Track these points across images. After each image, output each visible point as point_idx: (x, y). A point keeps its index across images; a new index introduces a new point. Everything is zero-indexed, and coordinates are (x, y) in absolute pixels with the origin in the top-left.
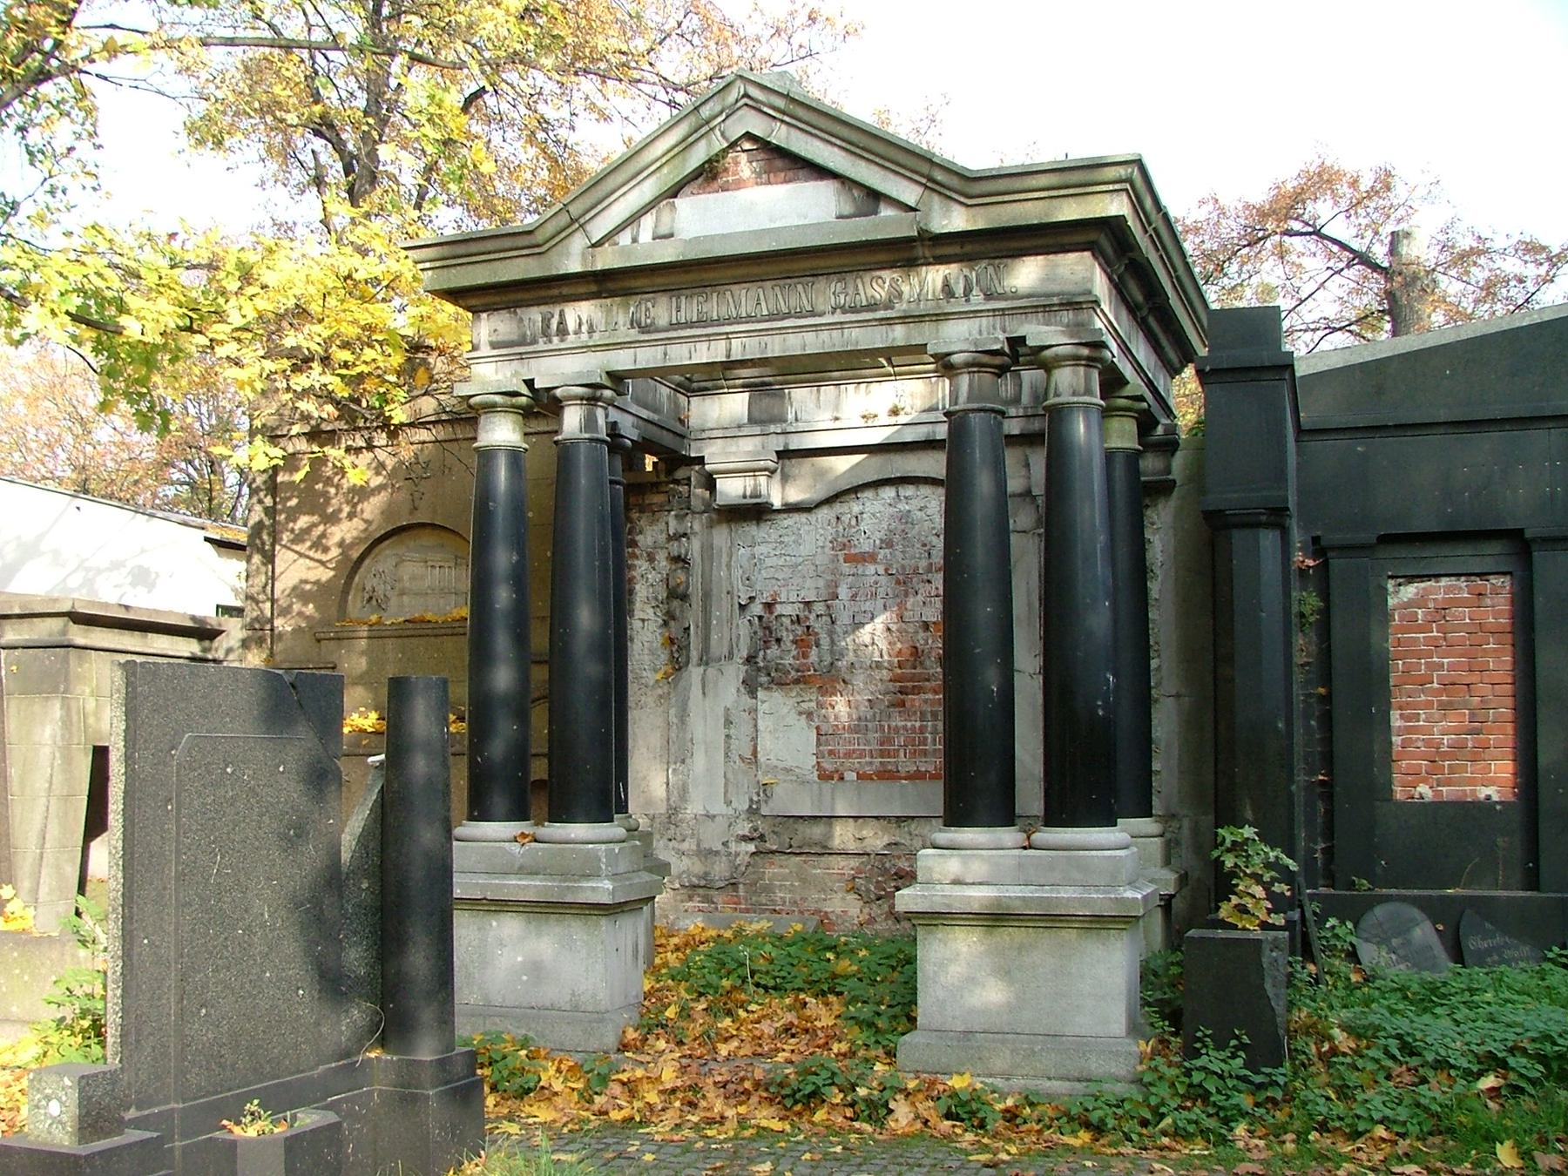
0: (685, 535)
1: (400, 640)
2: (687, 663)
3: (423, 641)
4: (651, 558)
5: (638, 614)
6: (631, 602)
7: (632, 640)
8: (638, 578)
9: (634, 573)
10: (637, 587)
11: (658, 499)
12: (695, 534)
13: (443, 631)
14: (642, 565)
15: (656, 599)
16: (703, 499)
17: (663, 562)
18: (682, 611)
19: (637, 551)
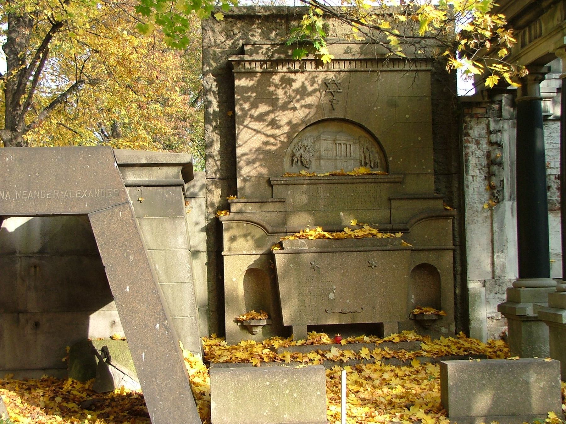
0: (499, 131)
1: (328, 186)
2: (503, 199)
3: (344, 186)
4: (478, 143)
5: (471, 173)
6: (467, 166)
7: (468, 187)
8: (470, 153)
9: (468, 151)
10: (470, 158)
11: (480, 111)
12: (505, 130)
13: (358, 181)
14: (472, 147)
15: (481, 165)
16: (509, 111)
17: (484, 145)
18: (499, 172)
19: (470, 139)
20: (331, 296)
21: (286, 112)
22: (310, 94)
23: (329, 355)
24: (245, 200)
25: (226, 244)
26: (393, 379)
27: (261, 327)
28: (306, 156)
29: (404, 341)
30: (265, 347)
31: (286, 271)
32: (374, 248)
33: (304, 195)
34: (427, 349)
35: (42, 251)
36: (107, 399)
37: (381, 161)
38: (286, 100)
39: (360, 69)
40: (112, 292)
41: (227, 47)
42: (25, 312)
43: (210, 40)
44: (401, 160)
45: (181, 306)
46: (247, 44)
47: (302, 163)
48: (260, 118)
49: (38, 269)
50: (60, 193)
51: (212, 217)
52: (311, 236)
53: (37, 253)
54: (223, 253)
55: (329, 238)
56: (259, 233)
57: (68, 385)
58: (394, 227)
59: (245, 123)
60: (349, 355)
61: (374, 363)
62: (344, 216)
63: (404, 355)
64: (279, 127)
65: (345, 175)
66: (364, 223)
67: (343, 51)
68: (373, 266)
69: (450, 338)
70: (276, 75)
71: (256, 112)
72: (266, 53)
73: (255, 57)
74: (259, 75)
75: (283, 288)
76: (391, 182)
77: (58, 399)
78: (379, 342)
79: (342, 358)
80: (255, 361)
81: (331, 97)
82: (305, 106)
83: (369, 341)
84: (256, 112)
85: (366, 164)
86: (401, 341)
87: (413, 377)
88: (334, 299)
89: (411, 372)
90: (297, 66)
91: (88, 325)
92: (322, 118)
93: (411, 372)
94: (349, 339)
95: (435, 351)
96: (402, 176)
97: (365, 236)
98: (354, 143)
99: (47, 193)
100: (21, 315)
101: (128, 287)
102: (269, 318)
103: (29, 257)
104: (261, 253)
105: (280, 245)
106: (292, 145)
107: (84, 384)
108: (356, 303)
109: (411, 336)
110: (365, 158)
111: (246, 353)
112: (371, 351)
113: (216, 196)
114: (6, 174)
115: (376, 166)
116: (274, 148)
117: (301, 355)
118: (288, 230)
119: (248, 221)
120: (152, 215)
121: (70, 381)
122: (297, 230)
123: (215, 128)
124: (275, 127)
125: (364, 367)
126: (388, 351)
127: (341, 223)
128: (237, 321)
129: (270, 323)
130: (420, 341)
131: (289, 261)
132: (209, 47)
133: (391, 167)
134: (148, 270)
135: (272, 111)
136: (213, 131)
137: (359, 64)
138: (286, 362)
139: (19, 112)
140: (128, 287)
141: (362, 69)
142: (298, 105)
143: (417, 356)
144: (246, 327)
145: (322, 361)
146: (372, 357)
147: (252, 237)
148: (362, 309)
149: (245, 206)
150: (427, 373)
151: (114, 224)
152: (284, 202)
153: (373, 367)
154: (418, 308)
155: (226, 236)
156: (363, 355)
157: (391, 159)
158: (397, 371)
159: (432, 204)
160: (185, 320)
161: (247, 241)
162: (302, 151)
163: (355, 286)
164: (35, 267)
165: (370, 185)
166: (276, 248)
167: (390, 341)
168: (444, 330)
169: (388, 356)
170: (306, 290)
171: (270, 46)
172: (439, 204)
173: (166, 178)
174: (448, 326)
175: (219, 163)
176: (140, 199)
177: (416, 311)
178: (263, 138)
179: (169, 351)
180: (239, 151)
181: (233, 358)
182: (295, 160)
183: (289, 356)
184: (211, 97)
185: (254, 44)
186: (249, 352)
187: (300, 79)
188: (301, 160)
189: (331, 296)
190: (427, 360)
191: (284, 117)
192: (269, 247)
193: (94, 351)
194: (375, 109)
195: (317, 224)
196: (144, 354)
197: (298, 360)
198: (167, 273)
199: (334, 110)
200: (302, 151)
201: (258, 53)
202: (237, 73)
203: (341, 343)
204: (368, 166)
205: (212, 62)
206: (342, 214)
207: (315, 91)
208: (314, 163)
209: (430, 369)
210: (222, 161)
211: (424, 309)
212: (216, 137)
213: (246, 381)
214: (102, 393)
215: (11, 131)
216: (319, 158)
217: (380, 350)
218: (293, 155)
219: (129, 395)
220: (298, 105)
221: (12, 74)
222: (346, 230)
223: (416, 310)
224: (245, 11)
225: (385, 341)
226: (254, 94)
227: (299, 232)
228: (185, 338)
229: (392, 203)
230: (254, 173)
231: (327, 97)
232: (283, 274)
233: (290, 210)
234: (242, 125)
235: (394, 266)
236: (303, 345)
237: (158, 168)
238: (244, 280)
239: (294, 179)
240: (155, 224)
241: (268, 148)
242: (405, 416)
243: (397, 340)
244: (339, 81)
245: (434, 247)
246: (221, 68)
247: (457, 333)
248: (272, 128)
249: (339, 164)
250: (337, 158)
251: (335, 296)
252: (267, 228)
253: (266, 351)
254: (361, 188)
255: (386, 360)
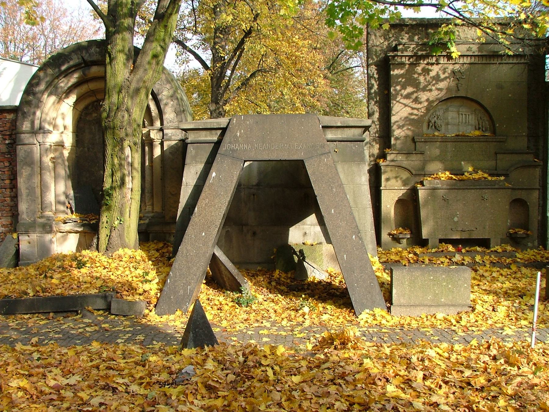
1: (454, 144)
3: (464, 144)
13: (475, 140)
20: (456, 219)
21: (425, 93)
22: (442, 80)
23: (454, 260)
24: (397, 152)
25: (383, 183)
26: (500, 277)
27: (406, 239)
28: (439, 122)
29: (505, 251)
30: (410, 253)
31: (426, 202)
32: (487, 187)
33: (437, 150)
34: (520, 257)
35: (258, 185)
36: (305, 285)
37: (490, 126)
38: (426, 84)
39: (477, 62)
40: (323, 213)
41: (385, 47)
42: (247, 225)
43: (373, 41)
45: (365, 224)
46: (400, 44)
47: (435, 127)
48: (408, 96)
49: (255, 196)
50: (284, 145)
51: (372, 163)
52: (443, 177)
53: (255, 186)
54: (381, 188)
55: (455, 179)
56: (405, 175)
57: (277, 273)
59: (398, 99)
60: (468, 259)
61: (485, 265)
62: (464, 164)
63: (505, 260)
64: (420, 103)
65: (465, 136)
66: (478, 169)
67: (465, 49)
69: (534, 250)
70: (419, 66)
71: (405, 92)
72: (413, 51)
73: (405, 54)
74: (407, 66)
75: (423, 213)
76: (498, 142)
77: (274, 283)
78: (488, 251)
79: (463, 261)
80: (404, 262)
81: (457, 82)
82: (438, 89)
83: (480, 251)
84: (405, 92)
85: (479, 129)
86: (503, 251)
87: (513, 276)
88: (457, 221)
89: (511, 272)
90: (434, 60)
91: (288, 235)
92: (450, 96)
93: (511, 272)
94: (467, 249)
95: (526, 258)
97: (479, 179)
98: (472, 114)
99: (275, 146)
100: (244, 227)
101: (333, 210)
102: (411, 233)
103: (250, 188)
104: (408, 188)
105: (422, 183)
106: (429, 114)
107: (287, 274)
109: (509, 248)
110: (479, 124)
111: (397, 256)
112: (482, 257)
113: (376, 150)
114: (248, 133)
115: (486, 130)
116: (416, 117)
117: (435, 258)
118: (427, 173)
119: (399, 167)
120: (344, 161)
121: (277, 272)
122: (433, 173)
123: (376, 102)
124: (417, 102)
125: (478, 268)
126: (494, 258)
127: (462, 169)
128: (390, 234)
129: (412, 236)
130: (515, 251)
131: (428, 195)
132: (373, 46)
134: (346, 198)
135: (416, 92)
136: (374, 105)
137: (477, 58)
138: (425, 263)
139: (220, 91)
140: (333, 210)
141: (479, 62)
142: (434, 88)
143: (515, 262)
144: (396, 239)
145: (450, 264)
146: (483, 261)
147: (401, 178)
149: (396, 156)
150: (522, 274)
151: (322, 167)
152: (423, 154)
153: (485, 269)
154: (512, 229)
155: (383, 177)
156: (477, 260)
157: (497, 125)
158: (502, 272)
159: (525, 157)
160: (368, 233)
161: (397, 181)
162: (435, 118)
164: (254, 195)
165: (483, 143)
166: (419, 185)
167: (495, 251)
168: (530, 244)
169: (494, 261)
170: (439, 215)
171: (415, 46)
172: (530, 158)
173: (353, 136)
174: (533, 242)
175: (378, 127)
176: (336, 150)
177: (511, 231)
178: (409, 110)
179: (362, 254)
180: (393, 119)
181: (389, 260)
182: (431, 125)
183: (427, 259)
184: (373, 82)
185: (404, 44)
186: (399, 256)
187: (435, 70)
188: (435, 125)
189: (456, 219)
190: (521, 264)
191: (424, 96)
192: (413, 184)
193: (295, 253)
194: (488, 90)
195: (445, 170)
196: (345, 255)
197: (433, 262)
198: (355, 201)
199: (459, 90)
200: (435, 118)
201: (407, 51)
202: (393, 64)
203: (462, 252)
204: (481, 130)
205: (374, 57)
206: (463, 163)
207: (446, 78)
208: (443, 127)
209: (524, 271)
210: (380, 125)
211: (517, 230)
212: (376, 108)
213: (417, 276)
214: (300, 281)
215: (216, 104)
216: (447, 124)
217: (488, 257)
218: (429, 122)
219: (320, 282)
220: (434, 88)
221: (217, 66)
222: (466, 174)
223: (511, 230)
224: (398, 21)
225: (492, 251)
226: (403, 80)
227: (434, 175)
228: (367, 245)
230: (403, 134)
231: (453, 82)
232: (423, 203)
234: (395, 100)
236: (436, 252)
237: (348, 129)
238: (395, 207)
239: (430, 138)
240: (346, 167)
241: (413, 117)
242: (522, 303)
243: (500, 250)
244: (463, 71)
245: (525, 187)
246: (380, 61)
247: (538, 247)
248: (416, 103)
249: (461, 128)
250: (460, 124)
252: (412, 171)
253: (411, 255)
254: (476, 145)
255: (493, 264)
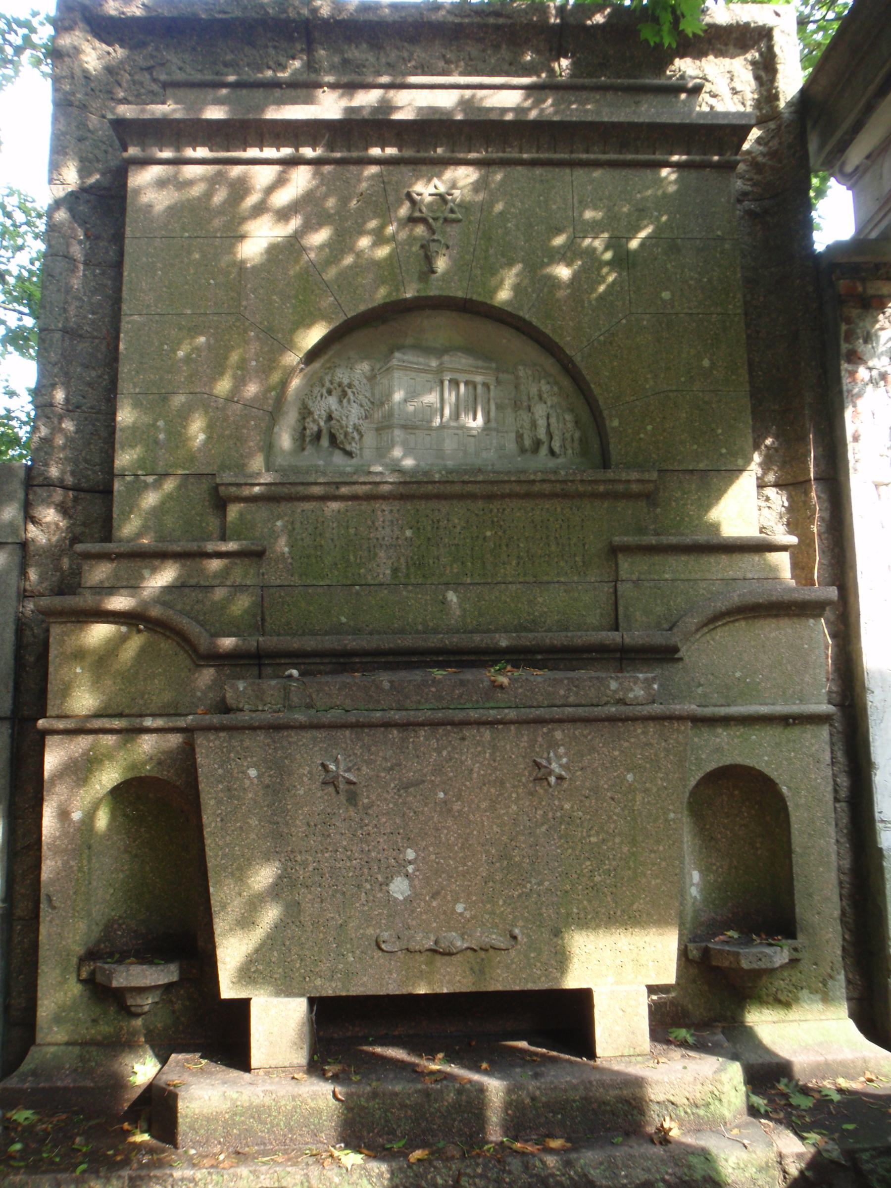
44: (649, 428)
47: (333, 438)
58: (627, 640)
68: (552, 780)
96: (655, 476)
108: (493, 913)
133: (615, 448)
148: (515, 938)
157: (616, 423)
163: (487, 852)
229: (620, 562)
233: (278, 582)
235: (630, 777)
251: (412, 886)
